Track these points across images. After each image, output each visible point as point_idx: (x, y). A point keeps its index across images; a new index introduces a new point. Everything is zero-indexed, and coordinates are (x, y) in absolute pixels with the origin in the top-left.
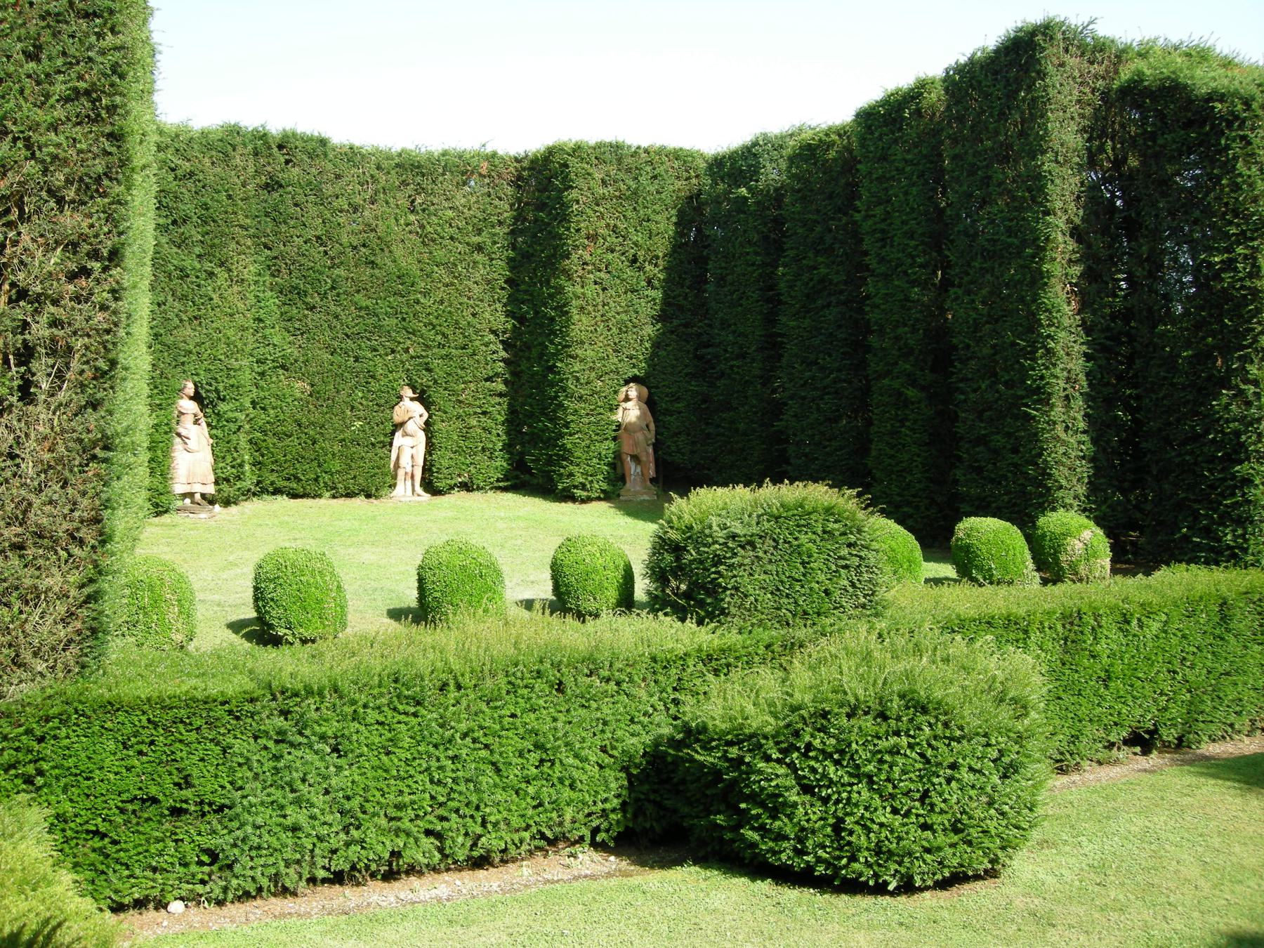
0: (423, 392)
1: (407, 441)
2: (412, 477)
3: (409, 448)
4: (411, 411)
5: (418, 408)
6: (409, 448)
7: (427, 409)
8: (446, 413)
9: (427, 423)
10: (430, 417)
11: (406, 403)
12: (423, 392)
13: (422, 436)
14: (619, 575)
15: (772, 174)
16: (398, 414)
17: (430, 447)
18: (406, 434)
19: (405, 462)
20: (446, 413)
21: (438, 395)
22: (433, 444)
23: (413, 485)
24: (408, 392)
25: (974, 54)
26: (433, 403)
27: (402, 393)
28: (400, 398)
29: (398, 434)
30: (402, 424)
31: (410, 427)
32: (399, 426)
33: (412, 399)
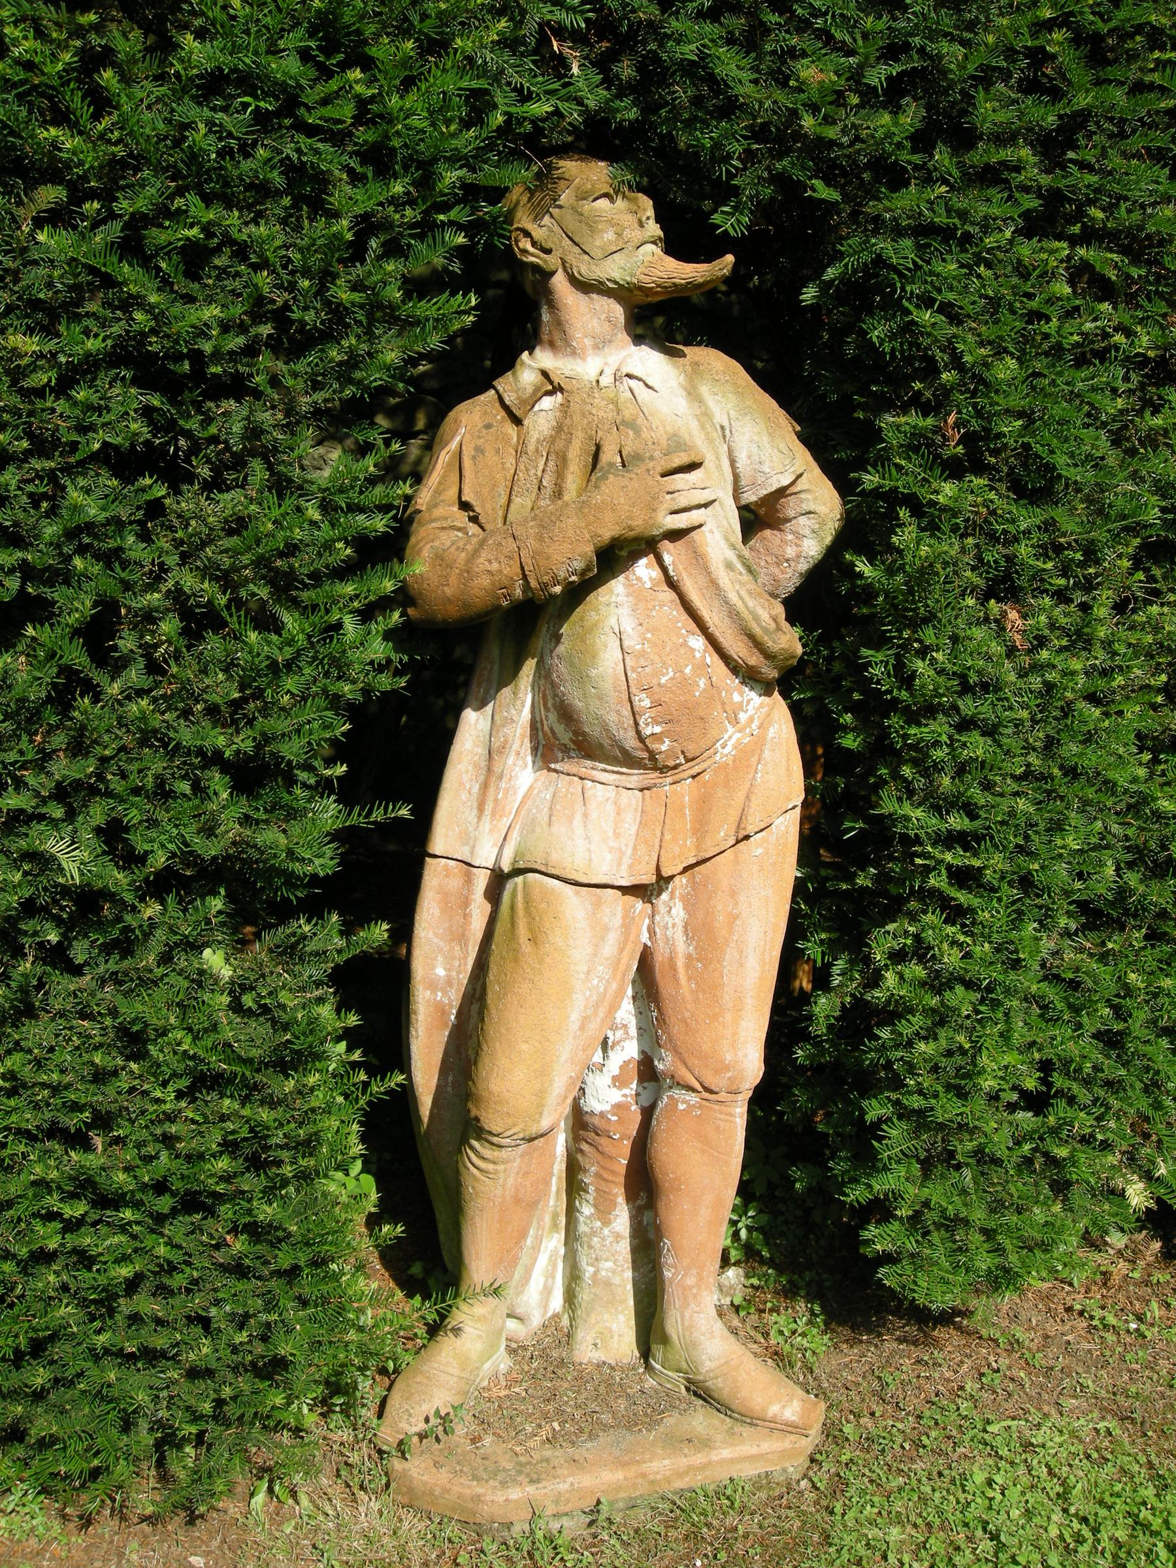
0: (791, 235)
1: (598, 825)
2: (643, 1184)
3: (615, 885)
4: (651, 452)
5: (716, 428)
6: (615, 885)
7: (835, 440)
8: (1035, 484)
9: (817, 600)
10: (863, 529)
11: (595, 360)
12: (791, 235)
13: (762, 752)
14: (697, 460)
15: (798, 428)
16: (482, 500)
17: (849, 874)
18: (566, 739)
19: (562, 1053)
20: (1035, 484)
21: (971, 286)
22: (883, 837)
23: (647, 1247)
24: (608, 232)
25: (796, 433)
26: (906, 375)
27: (537, 235)
28: (511, 314)
29: (489, 737)
30: (529, 622)
31: (625, 635)
32: (470, 649)
33: (660, 320)
